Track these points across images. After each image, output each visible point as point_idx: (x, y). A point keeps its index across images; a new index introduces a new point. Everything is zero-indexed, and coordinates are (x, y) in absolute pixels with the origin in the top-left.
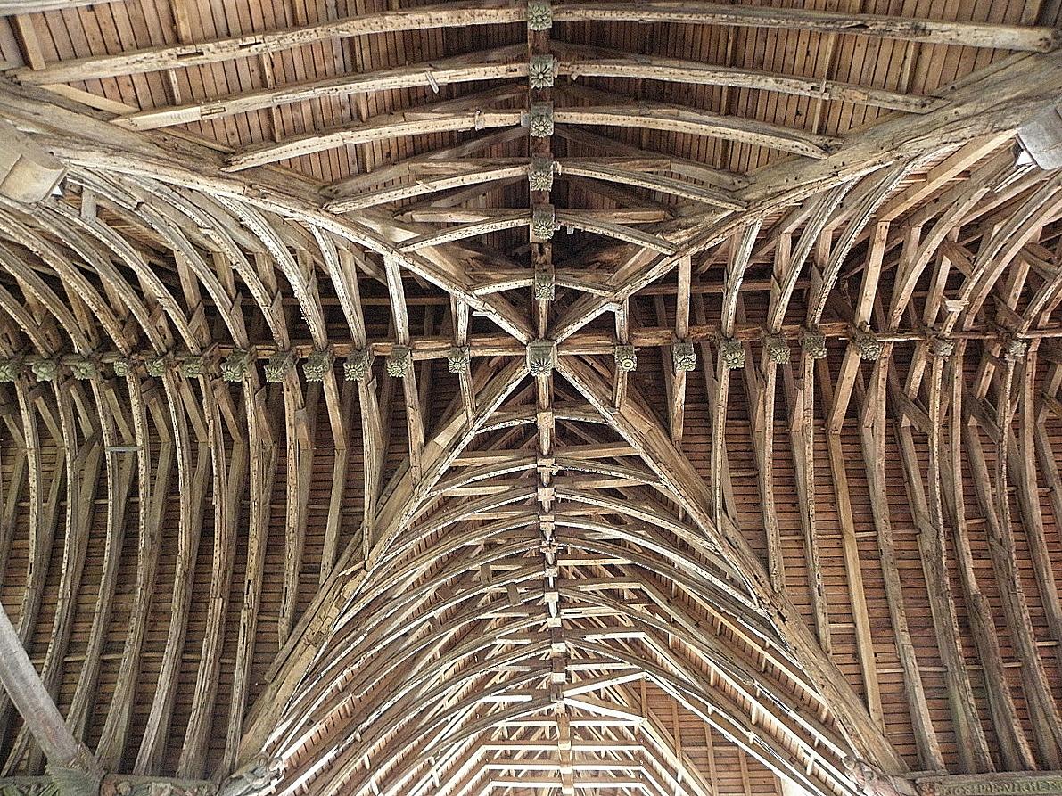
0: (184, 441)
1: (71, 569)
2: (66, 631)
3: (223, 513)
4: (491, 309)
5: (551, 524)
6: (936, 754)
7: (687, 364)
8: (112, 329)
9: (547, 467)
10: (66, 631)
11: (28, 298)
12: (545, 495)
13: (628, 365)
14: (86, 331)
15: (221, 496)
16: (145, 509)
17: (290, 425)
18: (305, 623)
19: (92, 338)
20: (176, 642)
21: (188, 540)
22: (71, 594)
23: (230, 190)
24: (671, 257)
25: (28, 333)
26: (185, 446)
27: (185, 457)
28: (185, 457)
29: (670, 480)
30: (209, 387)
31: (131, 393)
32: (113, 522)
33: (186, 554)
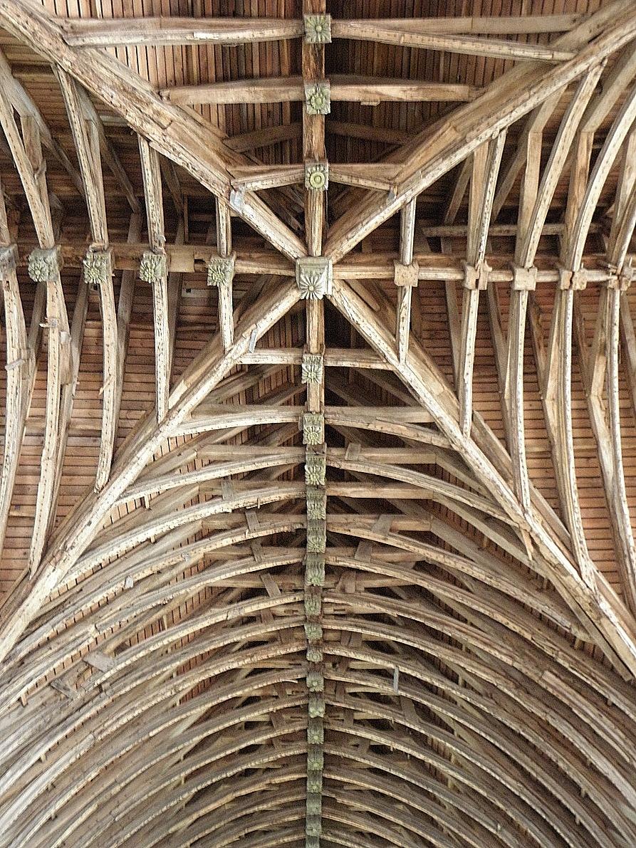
0: (392, 632)
1: (499, 771)
2: (552, 807)
3: (464, 630)
4: (250, 330)
5: (577, 275)
6: (268, 95)
7: (319, 101)
8: (276, 651)
9: (481, 274)
10: (552, 807)
11: (258, 694)
12: (526, 280)
13: (318, 179)
14: (291, 664)
15: (447, 625)
16: (453, 689)
17: (385, 539)
18: (579, 613)
19: (298, 662)
20: (576, 732)
21: (487, 670)
22: (522, 784)
23: (46, 577)
24: (149, 141)
25: (278, 708)
26: (397, 633)
27: (407, 637)
28: (407, 637)
29: (490, 126)
30: (339, 595)
31: (344, 654)
32: (462, 718)
33: (499, 678)
